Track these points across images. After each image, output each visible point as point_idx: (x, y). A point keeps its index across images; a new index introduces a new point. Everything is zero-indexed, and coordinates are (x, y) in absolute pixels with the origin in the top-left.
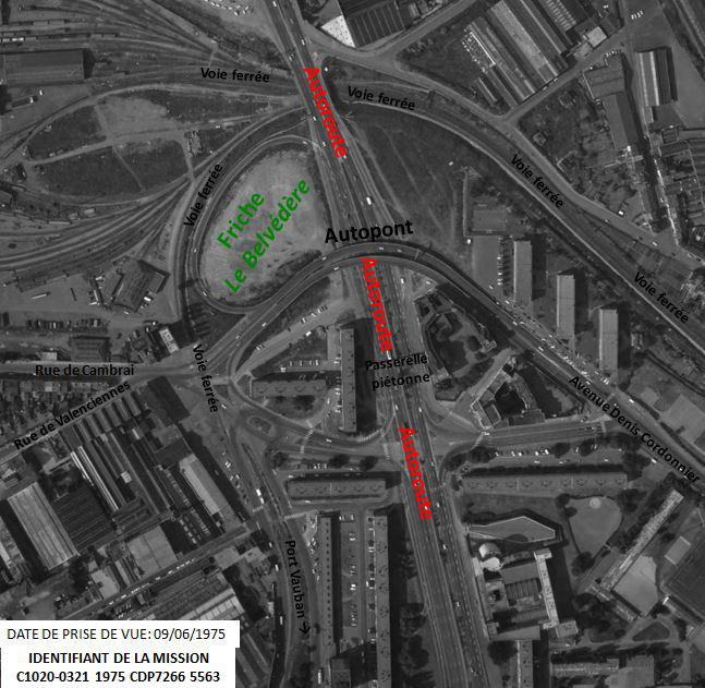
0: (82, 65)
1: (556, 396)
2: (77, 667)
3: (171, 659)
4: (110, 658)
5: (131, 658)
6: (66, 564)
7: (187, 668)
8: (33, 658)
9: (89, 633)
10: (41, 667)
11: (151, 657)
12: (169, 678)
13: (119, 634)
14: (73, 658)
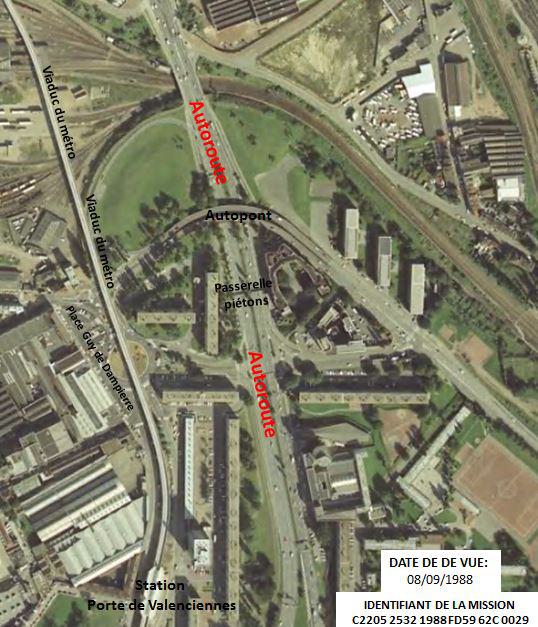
1: (337, 498)
3: (483, 606)
4: (432, 605)
5: (450, 606)
8: (469, 580)
10: (374, 612)
11: (467, 604)
12: (491, 621)
13: (458, 563)
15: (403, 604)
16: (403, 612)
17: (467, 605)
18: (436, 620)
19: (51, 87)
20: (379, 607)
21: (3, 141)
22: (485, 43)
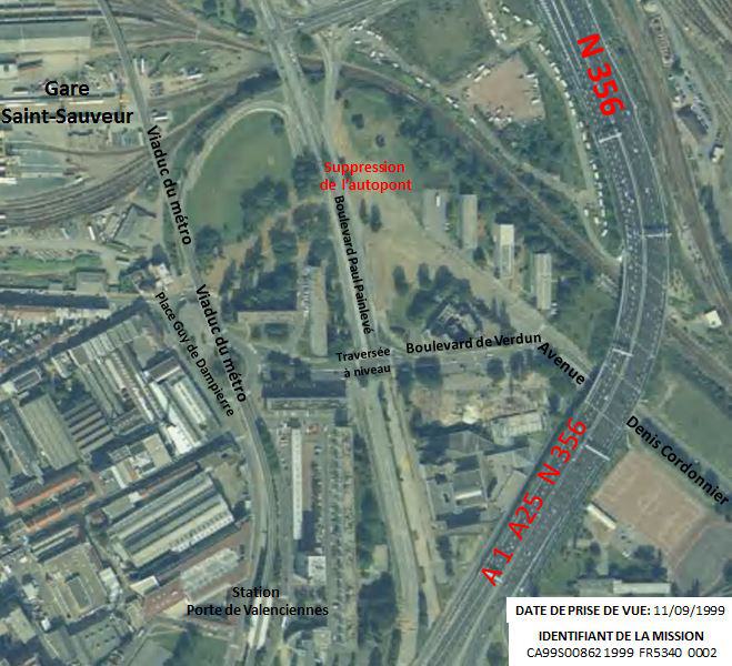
0: (84, 345)
2: (591, 644)
3: (587, 612)
5: (632, 637)
6: (415, 441)
7: (685, 645)
8: (542, 636)
9: (593, 609)
10: (550, 644)
11: (651, 636)
13: (620, 611)
14: (579, 636)
15: (582, 634)
16: (582, 644)
17: (651, 636)
18: (616, 652)
19: (158, 154)
20: (555, 638)
21: (3, 58)
22: (727, 19)
